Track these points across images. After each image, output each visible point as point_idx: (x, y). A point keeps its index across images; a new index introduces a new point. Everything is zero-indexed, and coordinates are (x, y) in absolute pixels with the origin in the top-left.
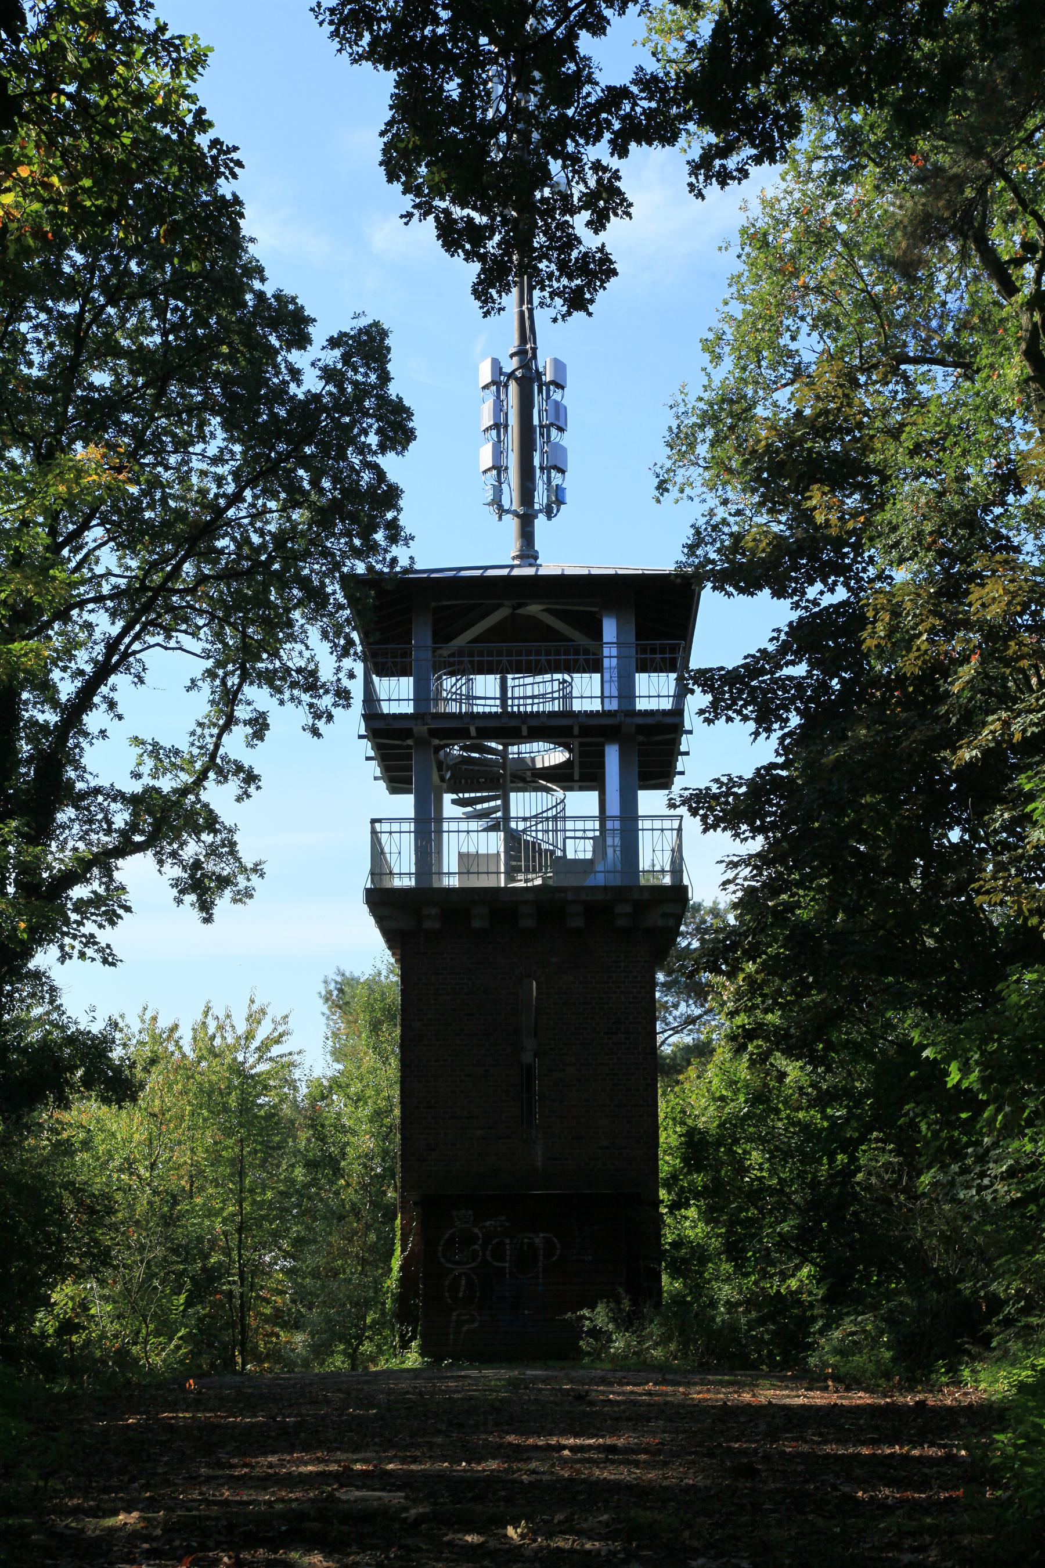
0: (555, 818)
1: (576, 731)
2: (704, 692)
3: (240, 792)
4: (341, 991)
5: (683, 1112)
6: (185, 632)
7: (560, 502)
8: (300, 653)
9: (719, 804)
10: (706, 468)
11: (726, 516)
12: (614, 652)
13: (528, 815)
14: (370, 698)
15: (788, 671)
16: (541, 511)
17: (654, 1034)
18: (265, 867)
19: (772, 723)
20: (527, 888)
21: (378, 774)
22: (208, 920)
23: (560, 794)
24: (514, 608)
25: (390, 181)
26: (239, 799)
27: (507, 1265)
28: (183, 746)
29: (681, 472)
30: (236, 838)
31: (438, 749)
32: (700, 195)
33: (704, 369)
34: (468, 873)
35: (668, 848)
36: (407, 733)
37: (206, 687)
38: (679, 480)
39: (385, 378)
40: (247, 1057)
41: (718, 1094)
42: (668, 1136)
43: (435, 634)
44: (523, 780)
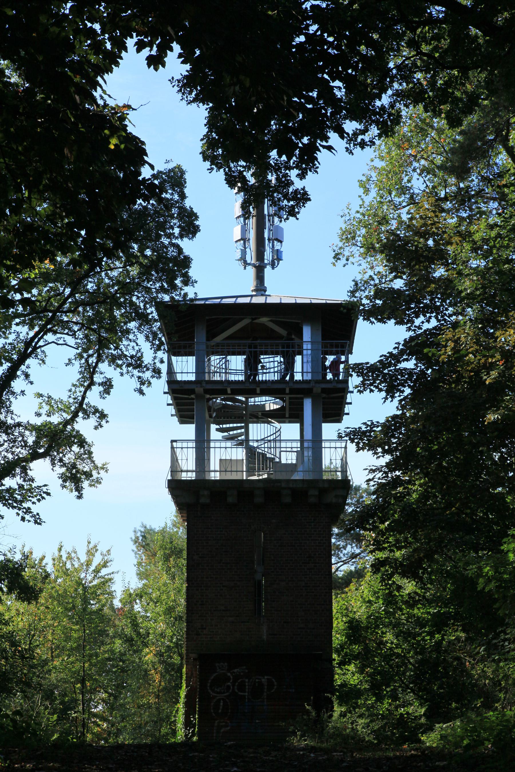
0: (275, 440)
1: (287, 391)
2: (358, 376)
3: (97, 424)
4: (144, 537)
5: (347, 609)
6: (67, 334)
7: (279, 259)
8: (133, 347)
9: (366, 436)
10: (361, 247)
11: (372, 274)
12: (309, 346)
13: (259, 439)
14: (171, 372)
15: (403, 365)
16: (269, 264)
17: (331, 564)
18: (108, 466)
19: (395, 393)
20: (259, 480)
21: (174, 412)
22: (80, 497)
23: (277, 425)
24: (253, 319)
25: (204, 161)
26: (96, 428)
27: (246, 694)
28: (65, 399)
29: (347, 249)
30: (92, 449)
31: (209, 400)
32: (351, 153)
33: (360, 196)
34: (226, 471)
35: (339, 458)
36: (192, 392)
37: (77, 364)
38: (347, 253)
39: (183, 196)
40: (87, 577)
41: (367, 599)
42: (338, 623)
43: (207, 332)
44: (257, 417)
